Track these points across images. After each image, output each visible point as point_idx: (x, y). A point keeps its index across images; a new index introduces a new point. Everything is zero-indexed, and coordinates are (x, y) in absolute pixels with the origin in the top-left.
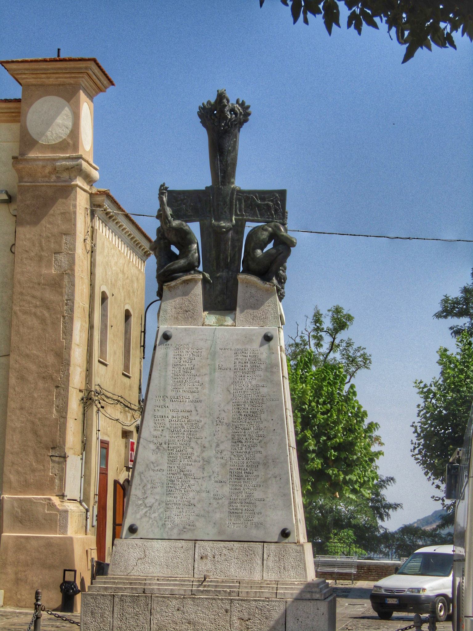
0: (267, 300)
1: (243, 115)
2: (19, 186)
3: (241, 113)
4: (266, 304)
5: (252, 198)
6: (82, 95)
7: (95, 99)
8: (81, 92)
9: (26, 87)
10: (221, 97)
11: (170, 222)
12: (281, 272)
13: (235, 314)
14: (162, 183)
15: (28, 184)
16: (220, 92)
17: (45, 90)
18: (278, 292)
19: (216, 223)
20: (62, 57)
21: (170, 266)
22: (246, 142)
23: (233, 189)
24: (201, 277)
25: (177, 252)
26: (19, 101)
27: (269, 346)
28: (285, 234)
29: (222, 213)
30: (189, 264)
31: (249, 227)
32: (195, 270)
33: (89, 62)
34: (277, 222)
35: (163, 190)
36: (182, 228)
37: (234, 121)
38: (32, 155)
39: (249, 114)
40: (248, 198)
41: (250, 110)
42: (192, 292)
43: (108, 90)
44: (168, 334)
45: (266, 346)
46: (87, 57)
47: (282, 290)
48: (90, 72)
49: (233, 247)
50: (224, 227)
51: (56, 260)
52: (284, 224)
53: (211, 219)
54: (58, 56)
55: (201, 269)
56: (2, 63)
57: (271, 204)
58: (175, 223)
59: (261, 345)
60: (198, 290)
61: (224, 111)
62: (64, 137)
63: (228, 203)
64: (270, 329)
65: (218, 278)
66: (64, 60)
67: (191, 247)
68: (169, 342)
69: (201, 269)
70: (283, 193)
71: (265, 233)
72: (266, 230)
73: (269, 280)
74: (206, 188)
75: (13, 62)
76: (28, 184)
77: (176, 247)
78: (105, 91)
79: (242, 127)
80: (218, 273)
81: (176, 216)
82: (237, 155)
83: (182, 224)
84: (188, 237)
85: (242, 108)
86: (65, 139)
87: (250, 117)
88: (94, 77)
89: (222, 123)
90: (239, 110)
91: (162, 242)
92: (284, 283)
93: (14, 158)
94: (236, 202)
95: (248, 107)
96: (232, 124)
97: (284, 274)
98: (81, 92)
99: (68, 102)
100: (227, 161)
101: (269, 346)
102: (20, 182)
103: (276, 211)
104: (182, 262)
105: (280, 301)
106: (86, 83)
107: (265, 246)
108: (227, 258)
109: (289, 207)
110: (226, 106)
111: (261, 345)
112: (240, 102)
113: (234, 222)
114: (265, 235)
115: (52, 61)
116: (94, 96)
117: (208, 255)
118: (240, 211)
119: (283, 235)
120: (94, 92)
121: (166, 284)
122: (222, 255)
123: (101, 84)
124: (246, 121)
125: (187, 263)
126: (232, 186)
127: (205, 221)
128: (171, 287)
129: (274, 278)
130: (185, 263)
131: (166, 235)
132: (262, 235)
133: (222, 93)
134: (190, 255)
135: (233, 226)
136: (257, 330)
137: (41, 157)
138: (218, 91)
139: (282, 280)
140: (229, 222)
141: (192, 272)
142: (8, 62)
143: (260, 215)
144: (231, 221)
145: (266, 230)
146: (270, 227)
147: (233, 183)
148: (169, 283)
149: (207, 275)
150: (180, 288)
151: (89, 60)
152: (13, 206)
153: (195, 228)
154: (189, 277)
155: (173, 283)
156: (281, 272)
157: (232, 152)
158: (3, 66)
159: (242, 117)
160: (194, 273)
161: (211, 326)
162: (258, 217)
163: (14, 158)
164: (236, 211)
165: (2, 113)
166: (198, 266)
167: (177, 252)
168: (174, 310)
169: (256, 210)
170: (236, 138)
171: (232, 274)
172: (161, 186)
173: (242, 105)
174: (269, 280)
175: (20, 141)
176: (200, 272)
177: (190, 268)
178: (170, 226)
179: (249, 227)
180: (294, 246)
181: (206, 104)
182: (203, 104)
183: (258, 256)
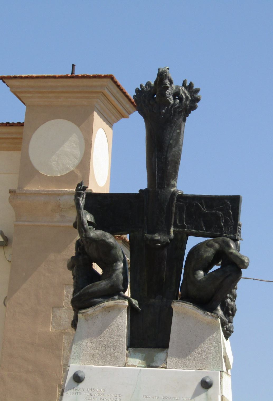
0: (209, 336)
1: (189, 100)
2: (16, 226)
3: (187, 97)
4: (207, 341)
5: (197, 205)
6: (97, 119)
7: (115, 125)
8: (95, 114)
9: (30, 109)
10: (162, 76)
11: (86, 231)
12: (229, 300)
13: (167, 353)
15: (26, 223)
16: (161, 70)
17: (54, 113)
18: (223, 326)
19: (149, 236)
20: (76, 74)
22: (194, 133)
23: (174, 194)
24: (127, 303)
25: (99, 270)
26: (20, 125)
27: (207, 395)
28: (234, 251)
30: (112, 286)
31: (193, 242)
33: (105, 80)
34: (226, 236)
35: (80, 190)
36: (104, 241)
37: (179, 107)
38: (30, 188)
39: (198, 100)
41: (199, 94)
42: (114, 322)
43: (131, 116)
44: (80, 375)
45: (203, 396)
46: (103, 74)
47: (230, 324)
48: (106, 92)
50: (158, 241)
51: (55, 316)
52: (235, 240)
54: (73, 73)
55: (128, 293)
56: (2, 78)
57: (221, 214)
58: (94, 233)
59: (196, 394)
60: (122, 320)
61: (165, 94)
62: (72, 169)
64: (209, 373)
66: (77, 77)
67: (116, 266)
68: (81, 385)
69: (128, 293)
70: (234, 202)
71: (209, 249)
72: (211, 246)
73: (212, 310)
74: (141, 191)
75: (15, 77)
76: (26, 223)
77: (99, 265)
78: (127, 117)
79: (188, 116)
81: (97, 225)
82: (180, 150)
83: (105, 236)
84: (113, 252)
85: (189, 91)
86: (73, 171)
87: (198, 104)
88: (112, 99)
89: (163, 111)
90: (185, 94)
91: (81, 258)
92: (233, 315)
93: (11, 192)
94: (176, 209)
95: (197, 91)
96: (174, 111)
97: (232, 303)
98: (95, 114)
99: (79, 125)
100: (166, 158)
101: (207, 395)
102: (17, 221)
103: (226, 222)
104: (103, 284)
105: (227, 338)
106: (102, 104)
107: (211, 267)
109: (243, 219)
110: (168, 88)
111: (196, 394)
112: (188, 84)
113: (172, 235)
114: (209, 253)
115: (66, 77)
116: (115, 122)
119: (232, 253)
120: (113, 117)
121: (82, 311)
123: (121, 108)
124: (193, 108)
125: (110, 285)
126: (172, 190)
129: (219, 308)
130: (107, 285)
131: (86, 250)
132: (206, 252)
133: (165, 72)
134: (114, 275)
135: (171, 240)
136: (193, 375)
137: (43, 191)
138: (159, 69)
139: (230, 312)
140: (165, 235)
141: (116, 297)
142: (9, 78)
143: (206, 227)
144: (169, 233)
145: (211, 246)
146: (217, 242)
147: (174, 186)
148: (85, 310)
149: (135, 302)
151: (105, 77)
152: (9, 250)
154: (110, 303)
156: (229, 300)
157: (174, 147)
158: (4, 82)
159: (188, 102)
160: (119, 299)
161: (135, 366)
162: (202, 230)
163: (11, 192)
165: (3, 138)
166: (124, 291)
167: (99, 270)
168: (90, 344)
170: (180, 129)
172: (79, 185)
173: (189, 87)
174: (212, 310)
175: (210, 248)
176: (125, 298)
177: (114, 292)
178: (85, 235)
179: (193, 242)
180: (246, 267)
181: (144, 85)
182: (141, 86)
183: (200, 279)
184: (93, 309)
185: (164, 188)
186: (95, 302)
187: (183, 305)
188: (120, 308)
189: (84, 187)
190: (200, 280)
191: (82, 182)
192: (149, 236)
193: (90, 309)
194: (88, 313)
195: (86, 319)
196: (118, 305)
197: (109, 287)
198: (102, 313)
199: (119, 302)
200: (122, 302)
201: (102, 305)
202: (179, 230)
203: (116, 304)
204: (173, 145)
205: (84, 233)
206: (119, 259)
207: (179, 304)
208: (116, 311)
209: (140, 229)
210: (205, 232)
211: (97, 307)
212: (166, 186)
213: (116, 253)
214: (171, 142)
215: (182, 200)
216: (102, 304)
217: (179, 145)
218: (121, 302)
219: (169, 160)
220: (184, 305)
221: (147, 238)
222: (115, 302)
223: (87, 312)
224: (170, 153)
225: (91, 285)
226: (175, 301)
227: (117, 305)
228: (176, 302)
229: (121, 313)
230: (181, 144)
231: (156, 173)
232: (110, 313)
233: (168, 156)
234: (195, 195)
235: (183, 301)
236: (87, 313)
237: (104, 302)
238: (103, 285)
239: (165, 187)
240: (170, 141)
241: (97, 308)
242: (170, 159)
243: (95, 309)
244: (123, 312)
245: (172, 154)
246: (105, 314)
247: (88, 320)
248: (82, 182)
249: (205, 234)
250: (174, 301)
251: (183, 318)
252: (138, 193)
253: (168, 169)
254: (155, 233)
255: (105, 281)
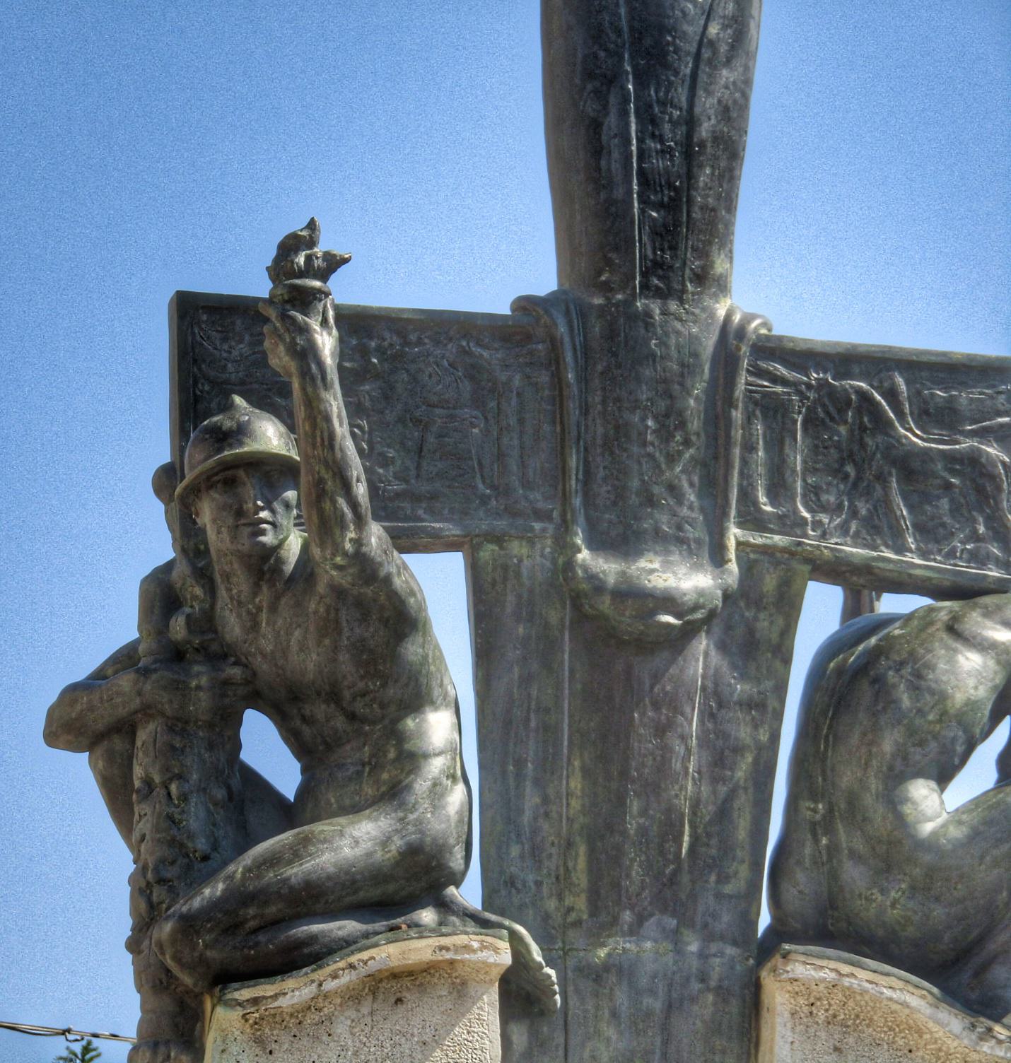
14: (297, 225)
19: (608, 568)
21: (273, 860)
23: (731, 335)
29: (651, 501)
32: (445, 906)
40: (835, 403)
49: (720, 754)
50: (668, 601)
53: (565, 527)
63: (695, 425)
65: (597, 975)
67: (421, 733)
69: (470, 893)
80: (597, 936)
84: (412, 650)
94: (749, 419)
100: (691, 122)
108: (671, 830)
117: (531, 800)
118: (773, 497)
121: (245, 994)
122: (635, 805)
125: (398, 843)
127: (517, 548)
128: (277, 1019)
130: (385, 842)
140: (697, 567)
141: (427, 916)
143: (920, 529)
144: (718, 559)
147: (722, 286)
148: (265, 989)
150: (341, 1028)
153: (439, 586)
155: (294, 991)
162: (901, 549)
164: (747, 496)
169: (887, 502)
171: (703, 956)
172: (290, 245)
177: (412, 882)
183: (927, 828)
184: (313, 981)
185: (680, 297)
186: (313, 939)
187: (847, 976)
188: (464, 984)
189: (328, 256)
190: (934, 833)
191: (312, 225)
192: (608, 568)
193: (290, 983)
194: (284, 1002)
195: (259, 1041)
196: (462, 961)
197: (394, 852)
198: (358, 1011)
199: (467, 948)
200: (483, 948)
201: (365, 963)
202: (768, 542)
203: (448, 956)
204: (723, 48)
205: (352, 527)
206: (436, 692)
207: (822, 967)
208: (441, 996)
209: (537, 526)
210: (918, 561)
211: (335, 971)
212: (691, 282)
213: (425, 657)
214: (713, 30)
215: (782, 370)
216: (365, 955)
217: (747, 54)
218: (476, 945)
219: (704, 134)
220: (853, 975)
221: (592, 577)
222: (441, 948)
223: (276, 997)
224: (709, 93)
225: (287, 837)
226: (795, 952)
227: (452, 963)
228: (802, 958)
229: (468, 1010)
230: (752, 48)
231: (632, 207)
232: (401, 1008)
233: (697, 110)
234: (855, 346)
235: (846, 955)
236: (276, 1004)
237: (376, 945)
238: (366, 846)
239: (684, 291)
240: (705, 27)
241: (334, 976)
242: (707, 131)
243: (320, 985)
244: (481, 1008)
245: (719, 101)
246: (372, 1013)
247: (274, 1046)
248: (312, 225)
249: (918, 572)
250: (789, 952)
251: (836, 1049)
252: (509, 313)
253: (701, 184)
254: (639, 554)
255: (369, 818)
